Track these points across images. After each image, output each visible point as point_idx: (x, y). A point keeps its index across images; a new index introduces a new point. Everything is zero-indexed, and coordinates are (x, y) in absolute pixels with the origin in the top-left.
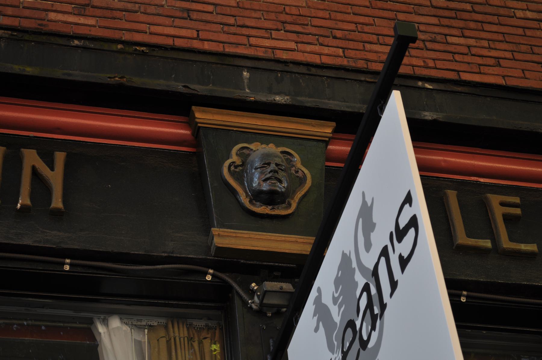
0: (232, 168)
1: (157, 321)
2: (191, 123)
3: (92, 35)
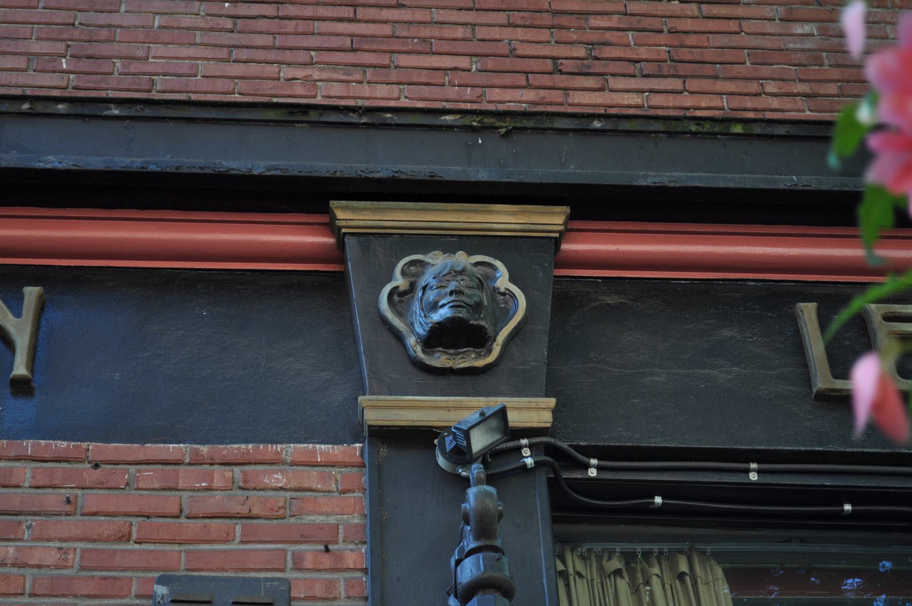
0: (396, 298)
2: (332, 227)
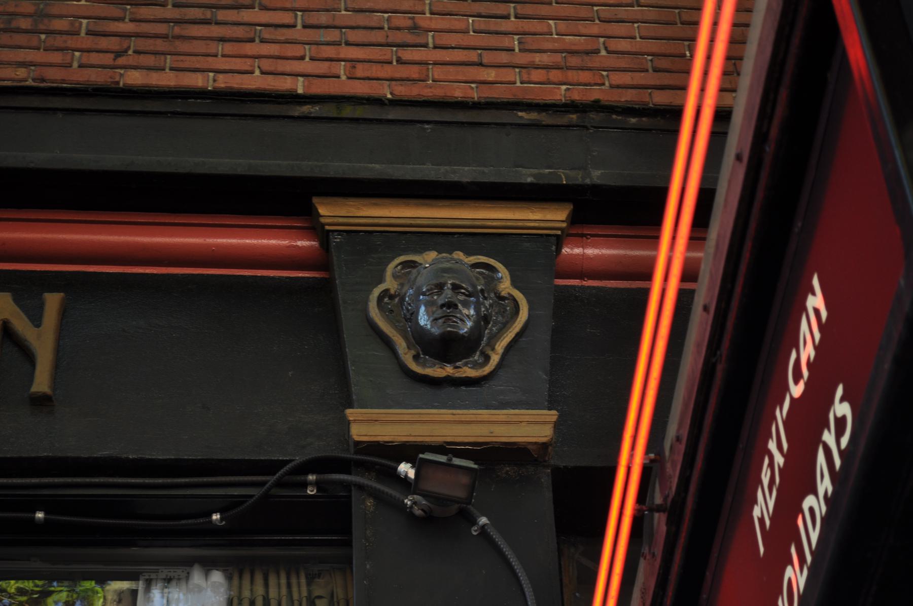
1: (186, 570)
2: (317, 230)
3: (455, 97)
